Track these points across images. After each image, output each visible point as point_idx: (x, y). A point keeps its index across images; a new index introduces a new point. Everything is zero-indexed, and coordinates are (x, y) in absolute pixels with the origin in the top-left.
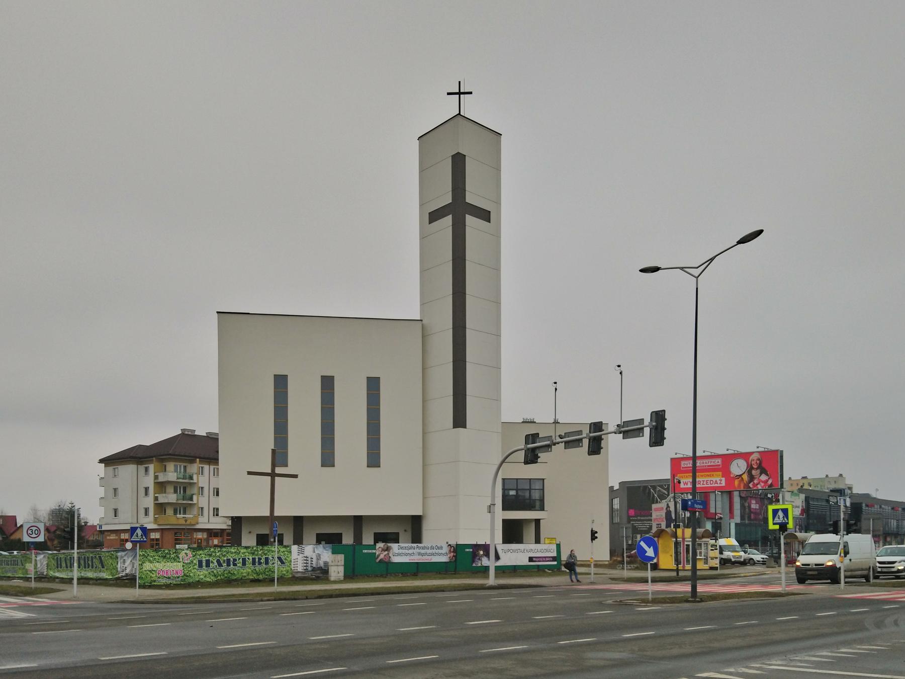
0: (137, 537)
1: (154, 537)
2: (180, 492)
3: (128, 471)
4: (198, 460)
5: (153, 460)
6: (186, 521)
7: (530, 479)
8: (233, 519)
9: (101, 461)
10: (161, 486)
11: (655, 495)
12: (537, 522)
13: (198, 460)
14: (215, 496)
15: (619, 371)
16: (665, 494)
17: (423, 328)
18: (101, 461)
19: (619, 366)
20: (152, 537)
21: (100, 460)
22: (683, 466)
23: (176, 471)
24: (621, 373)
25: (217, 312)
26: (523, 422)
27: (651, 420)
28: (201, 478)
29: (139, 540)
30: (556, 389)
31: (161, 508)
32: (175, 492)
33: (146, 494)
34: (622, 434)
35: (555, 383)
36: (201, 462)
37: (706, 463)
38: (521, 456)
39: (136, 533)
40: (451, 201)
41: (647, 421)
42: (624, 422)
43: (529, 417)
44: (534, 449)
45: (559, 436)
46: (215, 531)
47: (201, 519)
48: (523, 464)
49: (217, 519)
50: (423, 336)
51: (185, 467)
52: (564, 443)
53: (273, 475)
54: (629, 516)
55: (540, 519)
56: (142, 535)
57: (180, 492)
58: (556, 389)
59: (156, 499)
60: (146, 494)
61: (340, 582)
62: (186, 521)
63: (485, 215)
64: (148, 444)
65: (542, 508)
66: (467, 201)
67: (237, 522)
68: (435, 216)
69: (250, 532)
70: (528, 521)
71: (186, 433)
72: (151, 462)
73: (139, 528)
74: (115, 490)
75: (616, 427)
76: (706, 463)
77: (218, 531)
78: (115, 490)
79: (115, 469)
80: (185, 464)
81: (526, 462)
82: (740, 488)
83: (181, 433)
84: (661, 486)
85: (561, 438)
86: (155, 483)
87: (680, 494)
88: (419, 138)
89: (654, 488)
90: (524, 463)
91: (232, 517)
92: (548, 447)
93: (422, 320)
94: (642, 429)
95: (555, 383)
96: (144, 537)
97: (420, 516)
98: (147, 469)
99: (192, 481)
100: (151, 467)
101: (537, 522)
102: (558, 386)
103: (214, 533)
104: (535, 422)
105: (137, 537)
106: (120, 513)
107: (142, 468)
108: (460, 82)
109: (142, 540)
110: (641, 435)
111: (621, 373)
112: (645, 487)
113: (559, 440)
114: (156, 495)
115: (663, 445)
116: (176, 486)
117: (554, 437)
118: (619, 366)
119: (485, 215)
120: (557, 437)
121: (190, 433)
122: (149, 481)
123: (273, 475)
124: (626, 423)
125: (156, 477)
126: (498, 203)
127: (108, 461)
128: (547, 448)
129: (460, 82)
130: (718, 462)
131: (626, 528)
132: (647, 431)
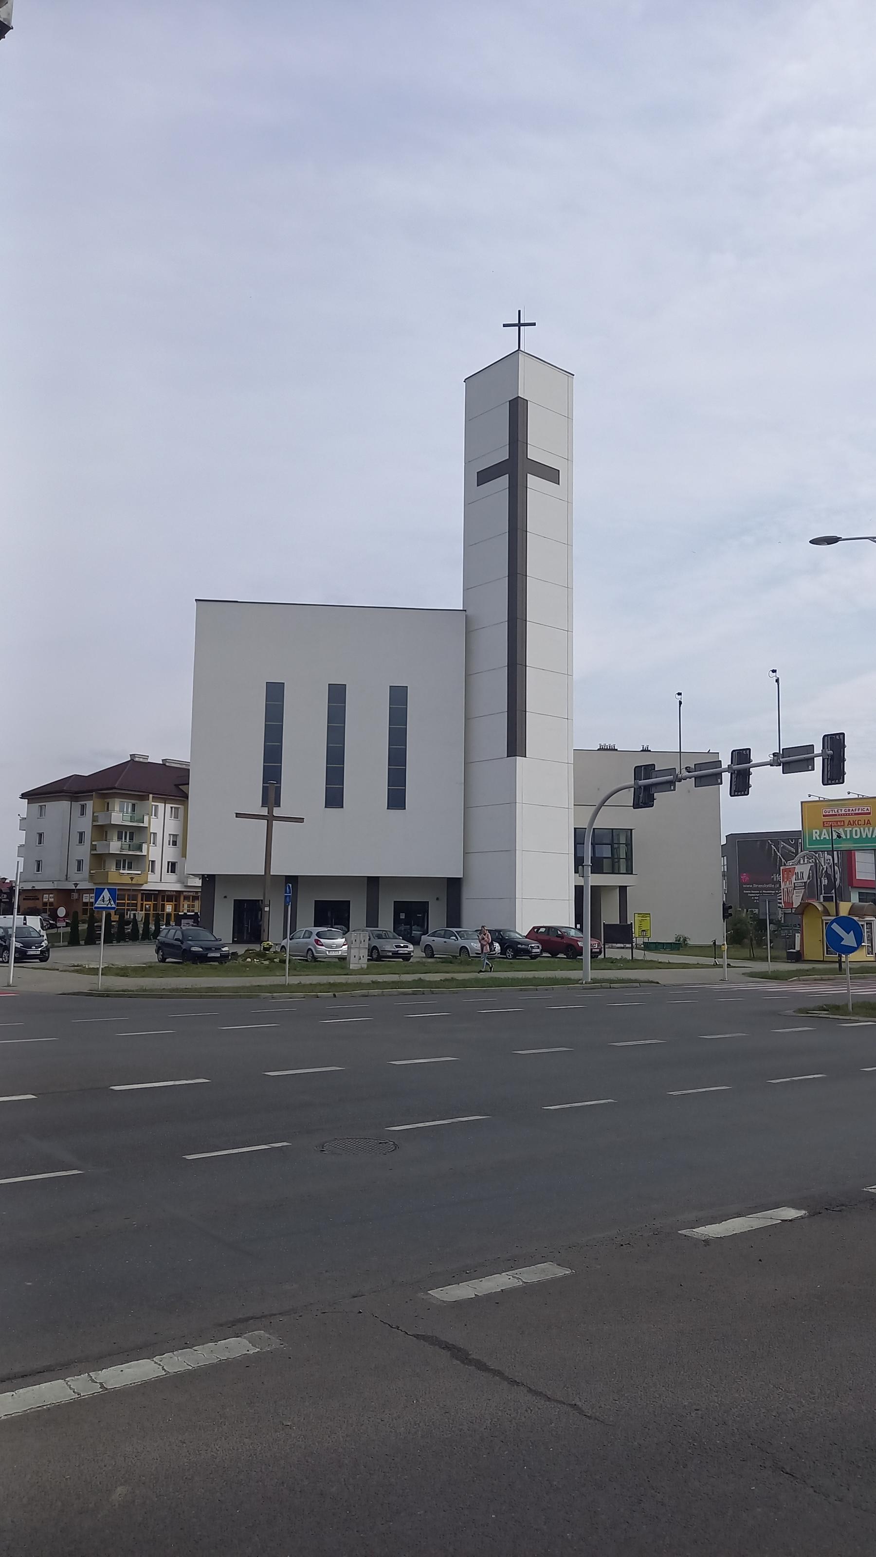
0: (103, 901)
1: (87, 900)
2: (125, 839)
3: (59, 808)
4: (151, 796)
5: (92, 795)
6: (132, 879)
7: (613, 829)
8: (203, 877)
9: (24, 796)
10: (102, 831)
11: (778, 854)
12: (623, 889)
13: (151, 796)
14: (171, 846)
15: (775, 679)
16: (793, 853)
17: (467, 619)
18: (24, 796)
19: (774, 671)
20: (84, 900)
21: (22, 794)
22: (824, 814)
23: (122, 811)
24: (777, 681)
25: (196, 600)
26: (642, 751)
27: (823, 748)
28: (153, 819)
29: (105, 906)
30: (680, 703)
31: (99, 859)
32: (119, 838)
33: (81, 841)
34: (781, 767)
35: (679, 694)
36: (154, 799)
37: (852, 810)
38: (628, 797)
39: (102, 896)
40: (508, 458)
41: (818, 749)
42: (783, 749)
43: (608, 743)
44: (647, 788)
45: (686, 768)
46: (169, 893)
47: (151, 877)
48: (632, 808)
49: (172, 877)
50: (468, 633)
51: (134, 805)
52: (694, 778)
53: (270, 819)
54: (741, 884)
55: (626, 886)
56: (110, 899)
57: (125, 839)
58: (680, 703)
59: (93, 847)
60: (81, 841)
61: (361, 972)
62: (132, 879)
63: (552, 475)
64: (86, 773)
65: (630, 871)
66: (508, 458)
67: (209, 880)
68: (484, 477)
69: (225, 897)
70: (611, 888)
71: (137, 759)
72: (90, 798)
73: (106, 889)
74: (40, 835)
75: (772, 756)
76: (852, 810)
77: (172, 893)
78: (40, 835)
79: (41, 806)
80: (134, 802)
81: (636, 806)
82: (830, 847)
83: (129, 759)
84: (786, 841)
85: (689, 772)
86: (93, 826)
87: (813, 853)
88: (465, 380)
89: (777, 844)
90: (633, 806)
91: (203, 875)
92: (669, 785)
93: (465, 610)
94: (812, 759)
95: (679, 694)
96: (112, 903)
97: (460, 879)
98: (83, 807)
99: (142, 825)
100: (89, 805)
101: (623, 889)
102: (683, 698)
103: (168, 896)
104: (650, 751)
105: (103, 901)
106: (43, 865)
107: (77, 805)
108: (519, 311)
109: (109, 906)
110: (810, 767)
111: (777, 681)
112: (763, 842)
113: (685, 773)
114: (93, 843)
115: (843, 783)
116: (122, 831)
117: (678, 771)
118: (774, 671)
119: (552, 475)
120: (684, 771)
121: (141, 760)
122: (85, 824)
123: (270, 819)
124: (787, 751)
125: (95, 819)
126: (569, 460)
127: (31, 796)
128: (668, 785)
129: (519, 311)
130: (867, 809)
131: (769, 902)
132: (818, 762)
